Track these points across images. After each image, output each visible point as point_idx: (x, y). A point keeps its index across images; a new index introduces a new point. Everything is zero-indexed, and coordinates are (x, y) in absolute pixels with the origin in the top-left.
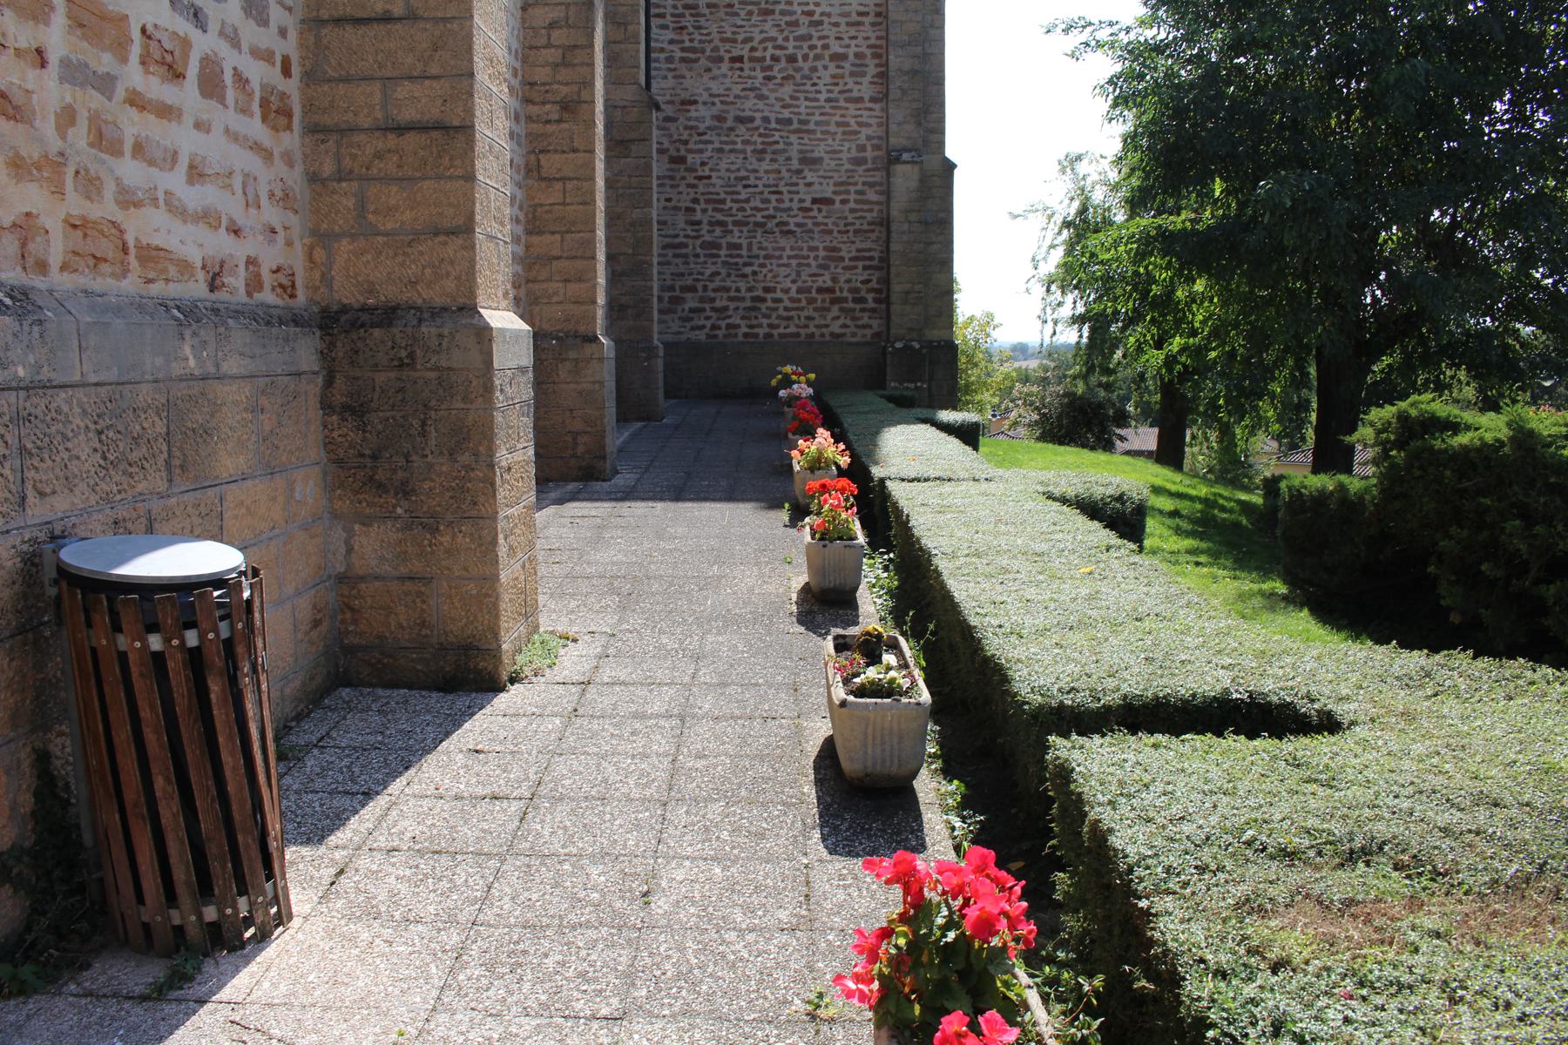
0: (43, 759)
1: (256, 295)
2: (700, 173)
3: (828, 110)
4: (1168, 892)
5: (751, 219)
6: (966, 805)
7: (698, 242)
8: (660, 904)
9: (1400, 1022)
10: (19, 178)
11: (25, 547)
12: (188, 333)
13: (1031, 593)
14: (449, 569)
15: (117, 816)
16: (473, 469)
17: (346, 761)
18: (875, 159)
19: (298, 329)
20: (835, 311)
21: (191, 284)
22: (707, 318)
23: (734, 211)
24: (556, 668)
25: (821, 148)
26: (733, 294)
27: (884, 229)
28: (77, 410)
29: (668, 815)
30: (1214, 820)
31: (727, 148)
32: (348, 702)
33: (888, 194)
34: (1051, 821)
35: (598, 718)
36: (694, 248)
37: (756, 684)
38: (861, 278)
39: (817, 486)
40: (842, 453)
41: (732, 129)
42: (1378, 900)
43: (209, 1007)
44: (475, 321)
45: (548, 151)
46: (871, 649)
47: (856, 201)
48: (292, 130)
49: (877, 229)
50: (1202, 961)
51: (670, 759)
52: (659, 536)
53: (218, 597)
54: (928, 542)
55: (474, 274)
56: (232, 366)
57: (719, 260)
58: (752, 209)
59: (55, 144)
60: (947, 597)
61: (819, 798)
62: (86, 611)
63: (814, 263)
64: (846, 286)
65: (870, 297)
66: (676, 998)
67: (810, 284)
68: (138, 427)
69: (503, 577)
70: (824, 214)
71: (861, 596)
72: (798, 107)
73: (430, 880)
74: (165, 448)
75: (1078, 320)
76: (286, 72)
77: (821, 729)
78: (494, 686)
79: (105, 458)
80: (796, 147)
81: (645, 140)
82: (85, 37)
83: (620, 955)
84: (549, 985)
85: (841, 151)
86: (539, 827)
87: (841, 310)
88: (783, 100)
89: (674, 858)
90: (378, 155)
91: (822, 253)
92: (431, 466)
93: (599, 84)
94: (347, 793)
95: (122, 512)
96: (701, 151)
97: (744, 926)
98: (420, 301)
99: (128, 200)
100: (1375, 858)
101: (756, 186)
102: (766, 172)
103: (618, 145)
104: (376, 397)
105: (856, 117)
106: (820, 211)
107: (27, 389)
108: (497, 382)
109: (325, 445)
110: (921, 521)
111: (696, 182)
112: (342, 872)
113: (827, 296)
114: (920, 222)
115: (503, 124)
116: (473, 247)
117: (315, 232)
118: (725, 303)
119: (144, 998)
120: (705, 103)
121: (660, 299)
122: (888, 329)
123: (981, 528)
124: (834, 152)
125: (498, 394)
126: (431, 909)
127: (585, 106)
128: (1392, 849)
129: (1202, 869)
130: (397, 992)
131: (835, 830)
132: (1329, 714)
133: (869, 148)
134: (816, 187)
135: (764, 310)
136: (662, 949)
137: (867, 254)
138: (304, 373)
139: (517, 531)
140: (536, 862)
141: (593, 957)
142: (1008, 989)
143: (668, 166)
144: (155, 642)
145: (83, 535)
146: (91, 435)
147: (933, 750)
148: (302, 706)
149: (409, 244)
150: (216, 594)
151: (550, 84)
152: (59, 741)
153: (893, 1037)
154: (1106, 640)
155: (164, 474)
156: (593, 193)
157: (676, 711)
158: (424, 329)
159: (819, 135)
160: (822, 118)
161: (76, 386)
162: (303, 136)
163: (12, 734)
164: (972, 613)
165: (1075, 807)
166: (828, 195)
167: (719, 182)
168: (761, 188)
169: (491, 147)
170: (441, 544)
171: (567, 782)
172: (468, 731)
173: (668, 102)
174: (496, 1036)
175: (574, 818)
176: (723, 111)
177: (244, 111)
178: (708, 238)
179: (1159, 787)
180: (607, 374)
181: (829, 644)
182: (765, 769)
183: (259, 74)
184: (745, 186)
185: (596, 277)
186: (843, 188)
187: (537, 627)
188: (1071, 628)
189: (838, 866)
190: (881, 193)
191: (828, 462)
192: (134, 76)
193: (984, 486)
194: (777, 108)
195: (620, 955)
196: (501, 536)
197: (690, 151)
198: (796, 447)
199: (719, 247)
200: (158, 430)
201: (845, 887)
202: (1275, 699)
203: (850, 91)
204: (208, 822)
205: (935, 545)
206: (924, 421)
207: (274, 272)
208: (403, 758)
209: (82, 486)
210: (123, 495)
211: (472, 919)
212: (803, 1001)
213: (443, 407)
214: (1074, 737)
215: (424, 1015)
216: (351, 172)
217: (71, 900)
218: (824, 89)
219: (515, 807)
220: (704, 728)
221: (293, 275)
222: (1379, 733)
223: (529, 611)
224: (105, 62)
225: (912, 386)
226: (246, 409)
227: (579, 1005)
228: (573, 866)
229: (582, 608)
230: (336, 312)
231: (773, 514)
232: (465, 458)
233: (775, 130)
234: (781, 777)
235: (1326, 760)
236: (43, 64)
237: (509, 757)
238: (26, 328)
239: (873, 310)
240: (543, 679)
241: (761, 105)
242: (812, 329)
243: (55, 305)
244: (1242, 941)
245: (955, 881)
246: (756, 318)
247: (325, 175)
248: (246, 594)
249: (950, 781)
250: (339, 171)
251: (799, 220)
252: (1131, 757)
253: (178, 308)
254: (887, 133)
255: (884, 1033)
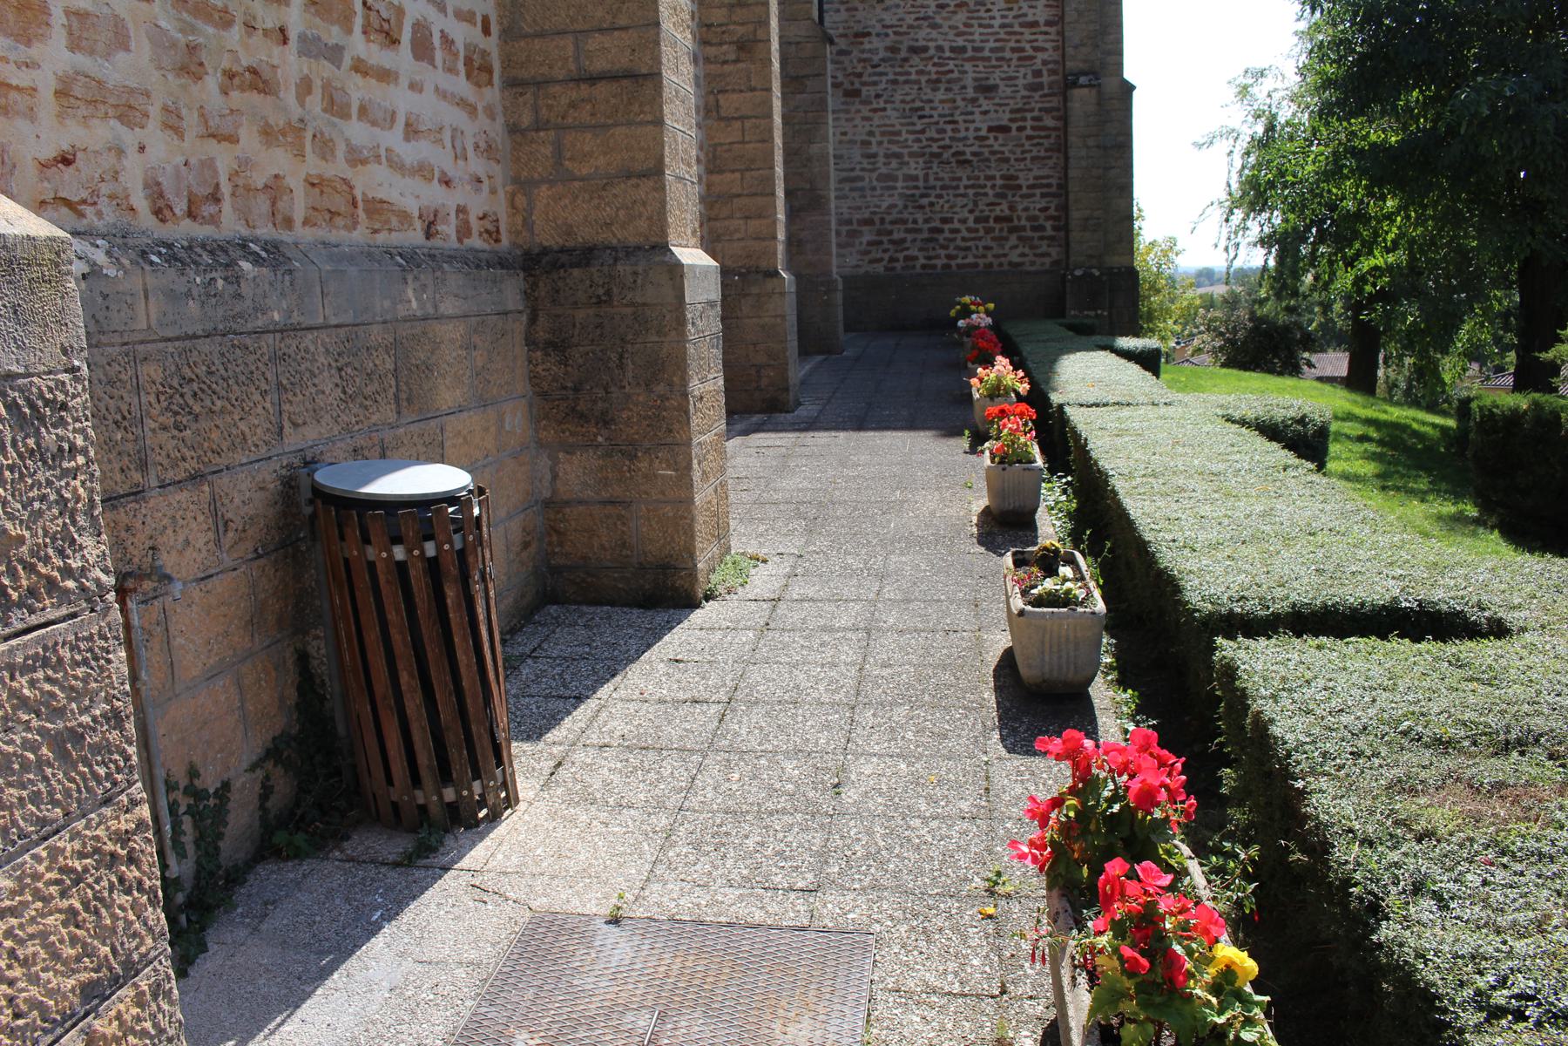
0: (303, 658)
1: (466, 241)
2: (875, 106)
3: (1002, 36)
4: (1325, 774)
5: (928, 150)
6: (1143, 709)
7: (875, 175)
8: (850, 795)
9: (1537, 885)
10: (268, 144)
11: (284, 472)
12: (410, 278)
13: (1205, 510)
14: (646, 493)
15: (369, 707)
16: (667, 399)
17: (558, 669)
18: (1050, 86)
19: (504, 271)
20: (1013, 240)
21: (411, 234)
22: (885, 251)
23: (910, 143)
24: (747, 586)
25: (996, 76)
26: (910, 226)
27: (1061, 156)
28: (321, 349)
29: (856, 717)
30: (1372, 712)
31: (901, 78)
32: (556, 618)
33: (1065, 119)
34: (1219, 719)
35: (789, 631)
36: (871, 181)
37: (938, 601)
38: (1038, 206)
39: (997, 411)
40: (1021, 380)
41: (905, 60)
42: (1528, 784)
43: (451, 873)
44: (667, 259)
45: (727, 91)
46: (1049, 563)
47: (1033, 128)
48: (493, 85)
49: (1055, 155)
50: (1351, 830)
51: (858, 667)
52: (843, 464)
53: (452, 513)
54: (1105, 464)
55: (665, 214)
56: (448, 307)
57: (896, 192)
58: (927, 140)
59: (296, 112)
60: (1123, 515)
61: (998, 703)
62: (340, 526)
63: (991, 192)
64: (1024, 215)
65: (1048, 225)
66: (866, 875)
67: (987, 213)
68: (371, 365)
69: (698, 499)
70: (1000, 141)
71: (1040, 518)
72: (971, 34)
73: (640, 772)
74: (393, 383)
75: (1265, 242)
76: (486, 31)
77: (1001, 641)
78: (690, 603)
79: (344, 392)
80: (971, 75)
81: (820, 75)
82: (317, 13)
83: (814, 838)
84: (749, 862)
85: (1017, 78)
86: (736, 727)
87: (1020, 238)
88: (957, 28)
89: (862, 754)
90: (573, 105)
91: (999, 182)
92: (628, 396)
93: (774, 23)
94: (560, 697)
95: (360, 441)
96: (875, 84)
97: (928, 815)
98: (615, 242)
99: (356, 158)
100: (1530, 749)
101: (931, 116)
102: (942, 101)
103: (792, 82)
104: (577, 332)
105: (1031, 41)
106: (996, 139)
107: (281, 331)
108: (689, 316)
109: (530, 379)
110: (1099, 443)
111: (871, 114)
112: (560, 764)
113: (1005, 225)
114: (1098, 147)
115: (687, 69)
116: (663, 188)
117: (516, 180)
118: (902, 235)
119: (396, 865)
120: (878, 35)
121: (838, 233)
122: (1068, 257)
123: (1158, 450)
124: (1011, 78)
125: (690, 327)
126: (642, 796)
127: (761, 45)
128: (1547, 741)
129: (1356, 755)
130: (614, 865)
131: (1014, 731)
132: (1499, 622)
133: (1045, 73)
134: (992, 115)
135: (941, 241)
136: (852, 833)
137: (1044, 181)
138: (511, 312)
139: (710, 457)
140: (734, 757)
141: (789, 839)
142: (1170, 857)
143: (843, 99)
144: (399, 553)
145: (330, 461)
146: (333, 371)
147: (1109, 660)
148: (515, 621)
149: (604, 188)
150: (450, 510)
151: (727, 25)
152: (315, 643)
153: (1063, 895)
154: (1278, 553)
155: (393, 407)
156: (770, 130)
157: (862, 625)
158: (619, 267)
159: (994, 62)
160: (997, 44)
161: (321, 328)
162: (502, 90)
163: (279, 636)
164: (1147, 529)
165: (1239, 700)
166: (1005, 123)
167: (895, 114)
168: (936, 118)
169: (677, 92)
170: (640, 469)
171: (761, 688)
172: (666, 643)
173: (841, 36)
174: (704, 903)
175: (769, 720)
176: (896, 42)
177: (451, 70)
178: (884, 170)
179: (1321, 683)
180: (788, 307)
181: (1008, 559)
182: (947, 677)
183: (463, 34)
184: (921, 117)
185: (776, 214)
186: (1018, 116)
187: (729, 548)
188: (1244, 542)
189: (1016, 763)
190: (1058, 119)
191: (1008, 390)
192: (359, 45)
193: (1163, 410)
194: (951, 37)
195: (814, 838)
196: (695, 461)
197: (865, 84)
198: (975, 375)
199: (895, 179)
200: (388, 366)
201: (1022, 782)
202: (1445, 607)
203: (1025, 15)
204: (446, 714)
205: (1112, 466)
206: (1103, 348)
207: (481, 219)
208: (609, 668)
209: (327, 418)
210: (360, 426)
211: (679, 805)
212: (983, 879)
213: (639, 340)
214: (1240, 639)
215: (639, 884)
216: (548, 121)
217: (331, 781)
218: (997, 15)
219: (714, 710)
220: (889, 640)
221: (497, 220)
222: (1547, 638)
223: (721, 533)
224: (334, 34)
225: (1092, 313)
226: (461, 347)
227: (778, 879)
228: (769, 761)
229: (770, 531)
230: (538, 255)
231: (953, 442)
232: (660, 388)
233: (949, 58)
234: (963, 684)
235: (1489, 661)
236: (285, 41)
237: (707, 666)
238: (279, 276)
239: (1052, 238)
240: (736, 597)
241: (934, 34)
242: (990, 259)
243: (301, 256)
244: (1389, 815)
245: (1120, 760)
246: (934, 249)
247: (524, 126)
248: (476, 511)
249: (1125, 691)
250: (537, 121)
251: (975, 149)
252: (1295, 656)
253: (401, 255)
254: (1063, 56)
255: (1055, 893)
